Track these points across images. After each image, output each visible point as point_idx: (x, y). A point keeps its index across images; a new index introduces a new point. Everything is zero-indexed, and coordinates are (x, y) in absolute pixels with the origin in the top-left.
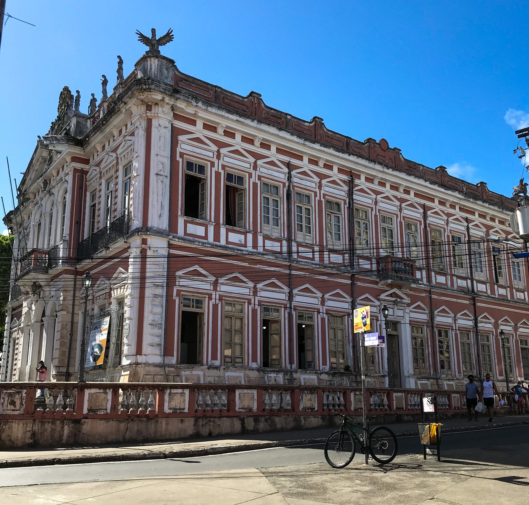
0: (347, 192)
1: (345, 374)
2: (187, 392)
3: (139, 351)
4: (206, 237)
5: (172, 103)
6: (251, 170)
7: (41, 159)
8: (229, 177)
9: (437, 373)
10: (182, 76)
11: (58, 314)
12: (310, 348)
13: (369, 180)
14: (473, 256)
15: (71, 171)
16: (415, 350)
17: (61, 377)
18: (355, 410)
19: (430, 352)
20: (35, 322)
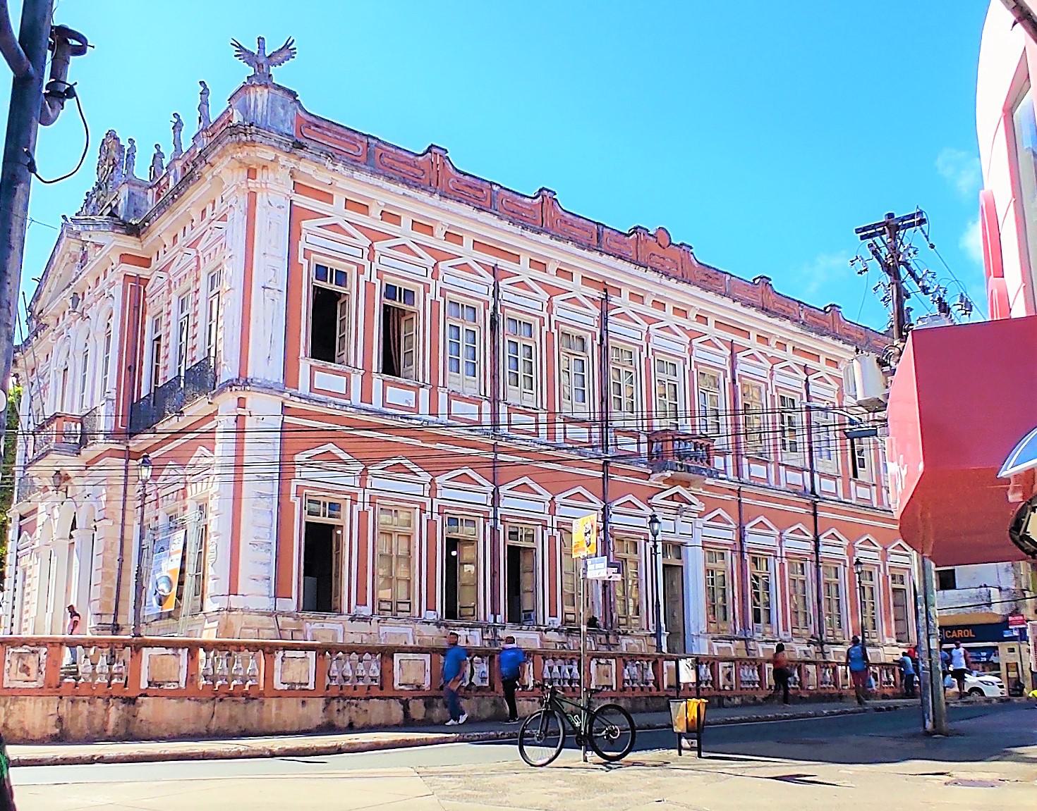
3: (233, 591)
4: (347, 396)
6: (429, 280)
8: (390, 291)
10: (313, 119)
11: (98, 525)
12: (529, 588)
13: (636, 297)
14: (814, 430)
15: (118, 279)
16: (711, 592)
19: (736, 595)
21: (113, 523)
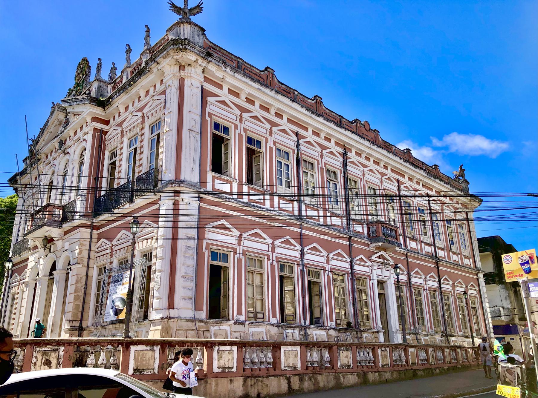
0: (342, 163)
1: (348, 330)
2: (235, 348)
3: (171, 305)
5: (204, 65)
7: (56, 121)
9: (416, 329)
12: (318, 304)
15: (91, 130)
17: (74, 331)
18: (382, 366)
20: (43, 276)
21: (82, 266)
